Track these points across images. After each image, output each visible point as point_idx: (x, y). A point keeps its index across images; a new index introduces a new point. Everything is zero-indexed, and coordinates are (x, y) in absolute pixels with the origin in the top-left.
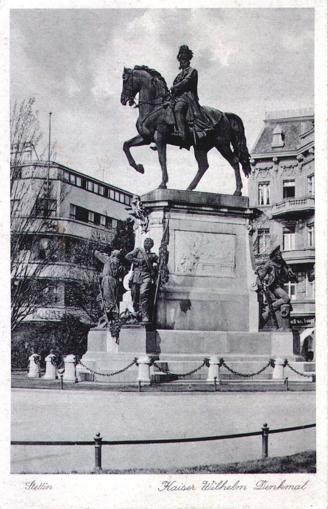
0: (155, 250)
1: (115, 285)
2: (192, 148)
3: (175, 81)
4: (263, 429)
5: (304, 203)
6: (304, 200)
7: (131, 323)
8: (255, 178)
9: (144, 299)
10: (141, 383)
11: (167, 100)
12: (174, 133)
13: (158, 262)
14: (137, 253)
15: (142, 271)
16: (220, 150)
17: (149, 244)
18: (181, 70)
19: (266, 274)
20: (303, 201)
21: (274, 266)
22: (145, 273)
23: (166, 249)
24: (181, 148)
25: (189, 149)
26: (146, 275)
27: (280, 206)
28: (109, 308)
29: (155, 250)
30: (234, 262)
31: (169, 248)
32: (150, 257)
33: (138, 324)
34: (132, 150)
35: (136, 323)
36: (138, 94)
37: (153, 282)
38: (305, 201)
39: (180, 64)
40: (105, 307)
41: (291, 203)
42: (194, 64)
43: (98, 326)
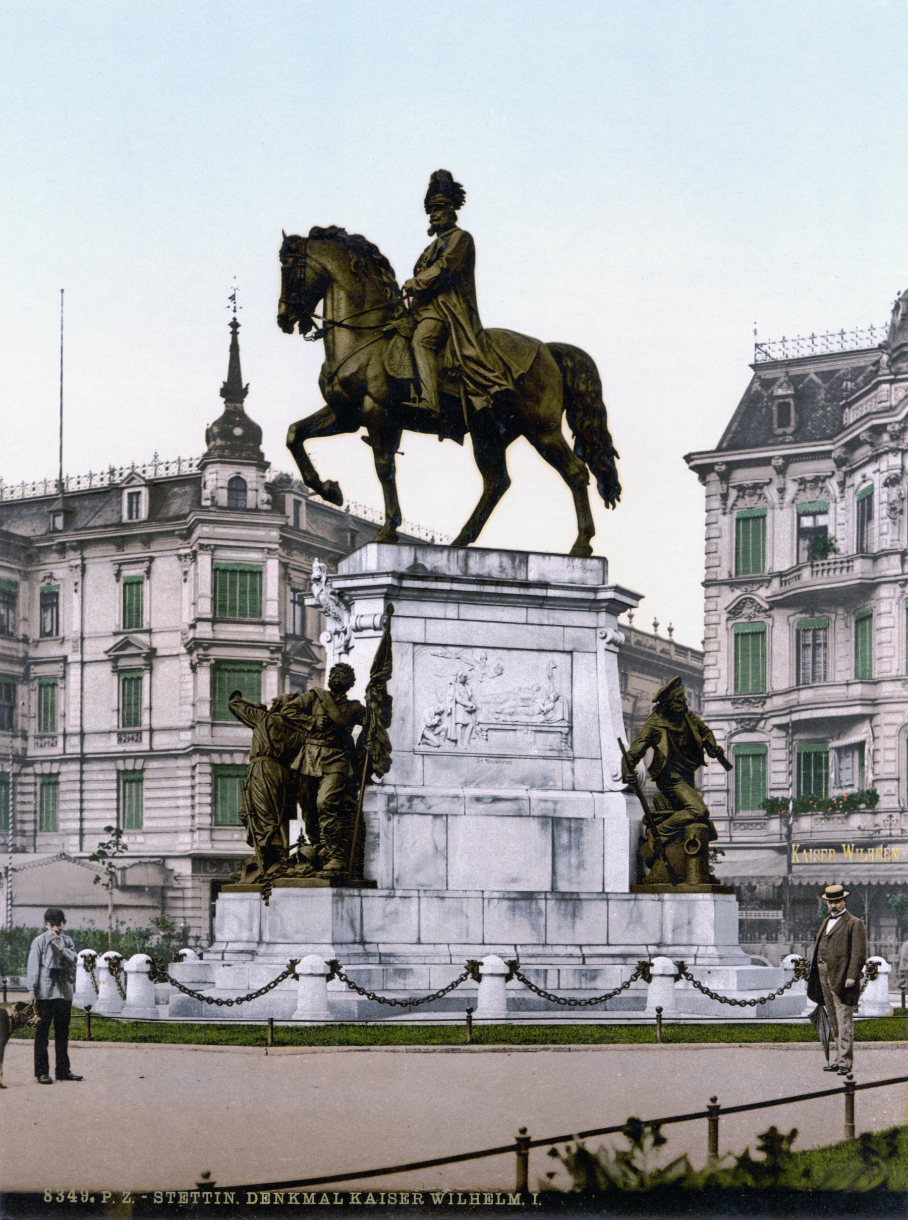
0: (357, 693)
1: (279, 781)
2: (468, 437)
6: (848, 562)
9: (325, 814)
10: (275, 1023)
11: (394, 318)
12: (409, 401)
13: (364, 723)
15: (322, 746)
18: (435, 237)
20: (846, 565)
23: (384, 691)
24: (441, 439)
25: (460, 441)
26: (333, 755)
27: (788, 578)
28: (264, 837)
29: (357, 693)
30: (567, 718)
31: (392, 687)
32: (344, 710)
34: (311, 446)
37: (351, 773)
38: (851, 564)
39: (431, 222)
40: (256, 833)
41: (815, 569)
42: (465, 219)
43: (242, 880)
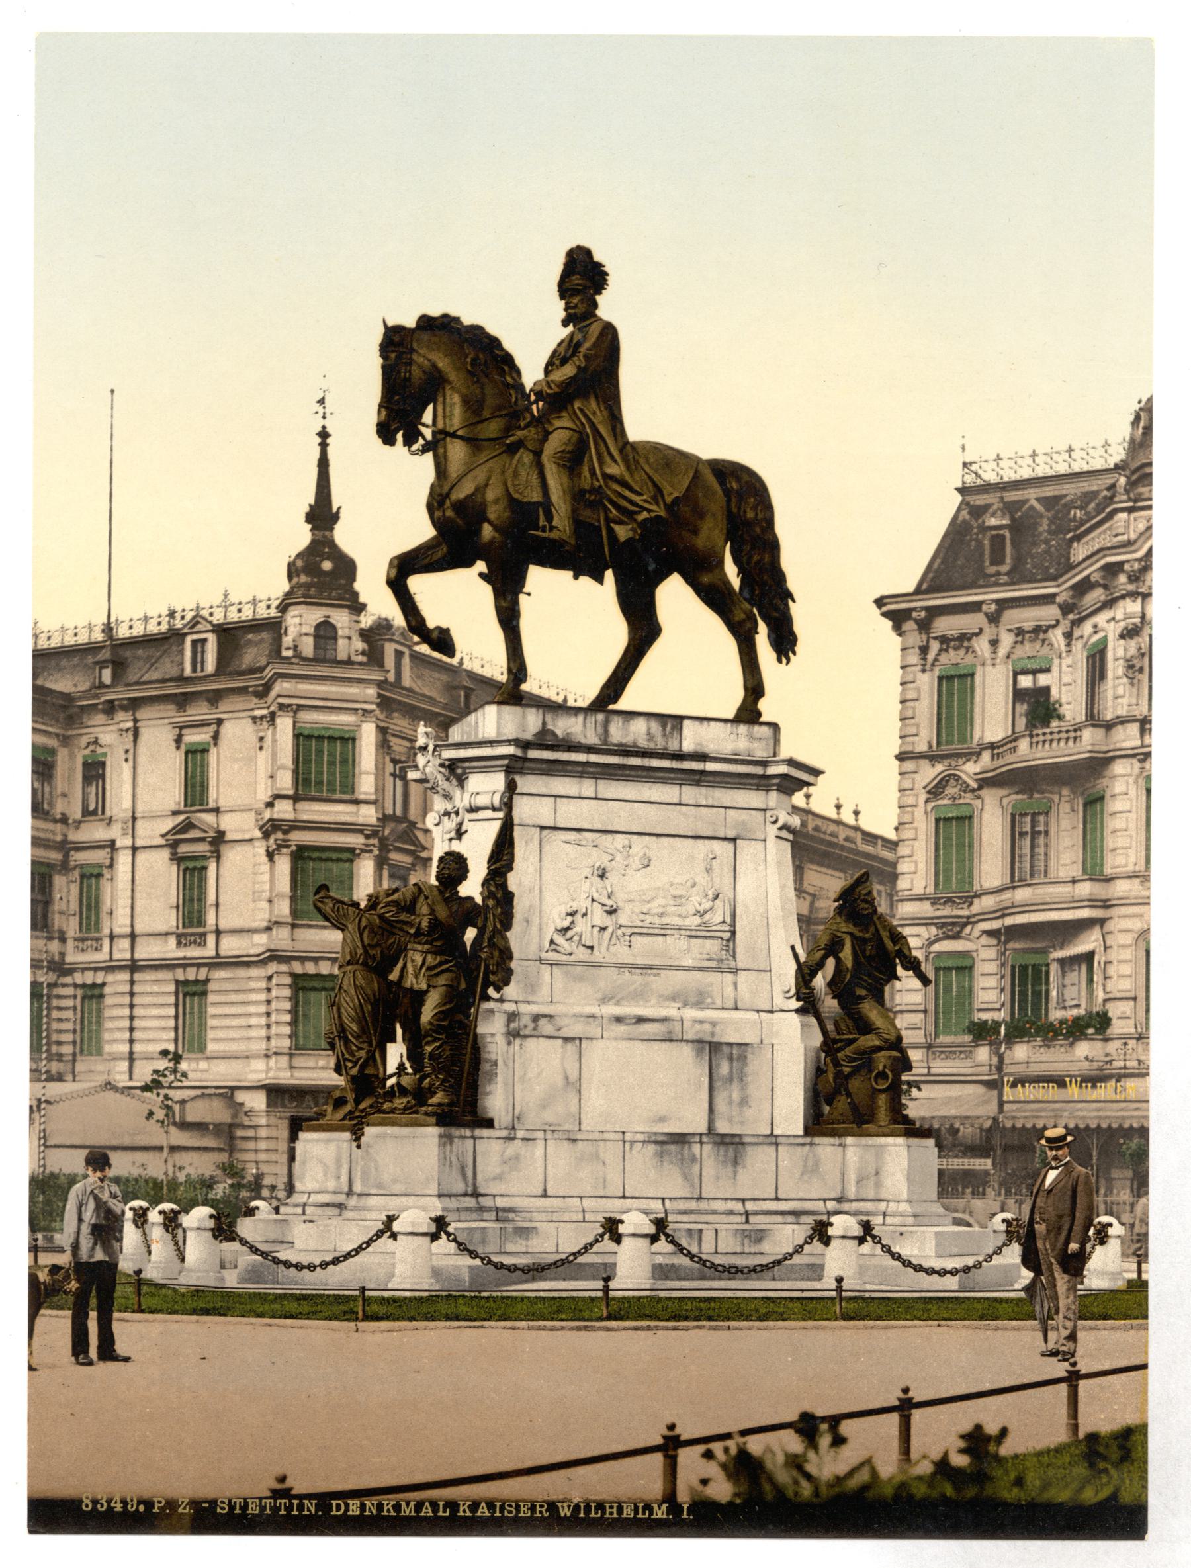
0: (471, 888)
2: (609, 575)
3: (555, 361)
4: (899, 1399)
5: (1075, 738)
6: (1075, 731)
7: (395, 1108)
8: (928, 667)
10: (367, 1293)
11: (519, 428)
13: (480, 925)
14: (414, 900)
15: (427, 952)
16: (691, 580)
17: (455, 867)
18: (571, 328)
19: (825, 957)
21: (850, 934)
22: (439, 959)
23: (504, 886)
24: (576, 577)
25: (600, 579)
26: (440, 964)
27: (1001, 750)
29: (471, 888)
30: (728, 920)
31: (514, 881)
33: (416, 1112)
35: (411, 1108)
36: (430, 408)
38: (1078, 733)
42: (608, 306)
